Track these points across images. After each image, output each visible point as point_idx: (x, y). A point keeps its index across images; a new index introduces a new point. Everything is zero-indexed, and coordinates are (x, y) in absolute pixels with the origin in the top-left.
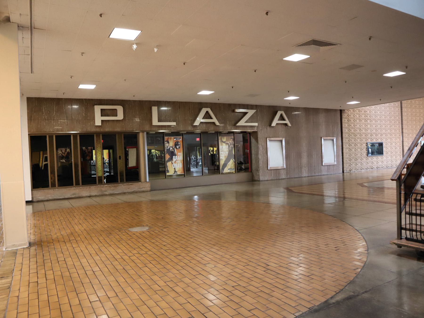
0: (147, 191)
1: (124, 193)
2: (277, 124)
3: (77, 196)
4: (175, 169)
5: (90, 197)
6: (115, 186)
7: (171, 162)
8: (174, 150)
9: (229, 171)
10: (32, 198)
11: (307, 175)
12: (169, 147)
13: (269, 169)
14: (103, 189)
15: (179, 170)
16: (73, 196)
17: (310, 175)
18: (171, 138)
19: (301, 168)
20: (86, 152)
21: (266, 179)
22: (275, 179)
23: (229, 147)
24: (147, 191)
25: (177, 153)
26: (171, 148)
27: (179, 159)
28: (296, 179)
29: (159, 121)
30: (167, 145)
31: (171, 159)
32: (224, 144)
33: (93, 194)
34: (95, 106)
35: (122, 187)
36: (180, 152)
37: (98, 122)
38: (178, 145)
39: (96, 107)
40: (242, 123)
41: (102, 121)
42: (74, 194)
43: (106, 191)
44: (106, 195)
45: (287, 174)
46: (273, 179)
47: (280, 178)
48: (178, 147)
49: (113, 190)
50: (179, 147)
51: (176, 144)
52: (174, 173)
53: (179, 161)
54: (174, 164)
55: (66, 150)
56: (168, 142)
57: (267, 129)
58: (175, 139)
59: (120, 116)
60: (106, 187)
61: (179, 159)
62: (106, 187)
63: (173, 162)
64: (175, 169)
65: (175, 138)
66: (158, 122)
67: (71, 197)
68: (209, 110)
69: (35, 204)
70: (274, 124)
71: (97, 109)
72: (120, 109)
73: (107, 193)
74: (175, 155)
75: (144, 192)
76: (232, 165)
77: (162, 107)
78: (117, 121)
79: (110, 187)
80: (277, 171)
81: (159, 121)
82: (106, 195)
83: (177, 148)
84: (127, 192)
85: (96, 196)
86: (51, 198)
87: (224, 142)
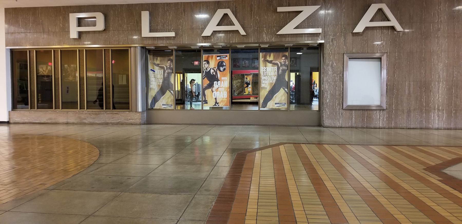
0: (136, 124)
1: (107, 124)
2: (367, 28)
3: (53, 121)
4: (216, 99)
5: (67, 124)
6: (96, 114)
7: (210, 90)
8: (216, 73)
9: (276, 107)
10: (9, 119)
11: (442, 125)
12: (208, 70)
13: (344, 107)
14: (83, 116)
15: (222, 101)
16: (49, 121)
17: (452, 126)
18: (212, 56)
19: (428, 112)
20: (69, 70)
21: (338, 124)
22: (360, 125)
23: (278, 69)
24: (136, 124)
25: (221, 77)
26: (212, 71)
27: (222, 85)
28: (412, 132)
29: (151, 31)
30: (207, 66)
31: (247, 86)
32: (269, 65)
33: (71, 121)
34: (70, 14)
35: (106, 116)
36: (225, 76)
37: (74, 34)
38: (223, 66)
39: (71, 15)
40: (289, 29)
41: (80, 33)
42: (50, 119)
43: (85, 119)
44: (85, 124)
45: (389, 119)
46: (354, 125)
47: (372, 126)
48: (222, 69)
49: (94, 118)
50: (224, 69)
51: (220, 64)
52: (215, 105)
53: (223, 89)
54: (215, 92)
55: (47, 67)
56: (208, 63)
57: (345, 38)
58: (219, 58)
59: (100, 26)
60: (86, 113)
61: (222, 85)
62: (86, 113)
63: (214, 89)
64: (216, 99)
65: (218, 56)
66: (150, 31)
67: (47, 122)
68: (228, 12)
69: (12, 126)
70: (359, 28)
71: (73, 18)
72: (100, 18)
73: (86, 122)
74: (218, 80)
75: (132, 124)
76: (283, 98)
77: (200, 12)
78: (94, 32)
79: (90, 114)
80: (364, 110)
81: (151, 31)
82: (85, 124)
83: (220, 71)
84: (111, 123)
85: (73, 124)
86: (27, 121)
87: (270, 62)
